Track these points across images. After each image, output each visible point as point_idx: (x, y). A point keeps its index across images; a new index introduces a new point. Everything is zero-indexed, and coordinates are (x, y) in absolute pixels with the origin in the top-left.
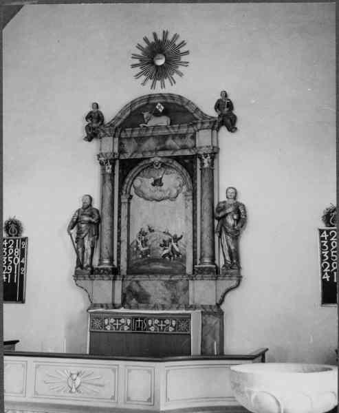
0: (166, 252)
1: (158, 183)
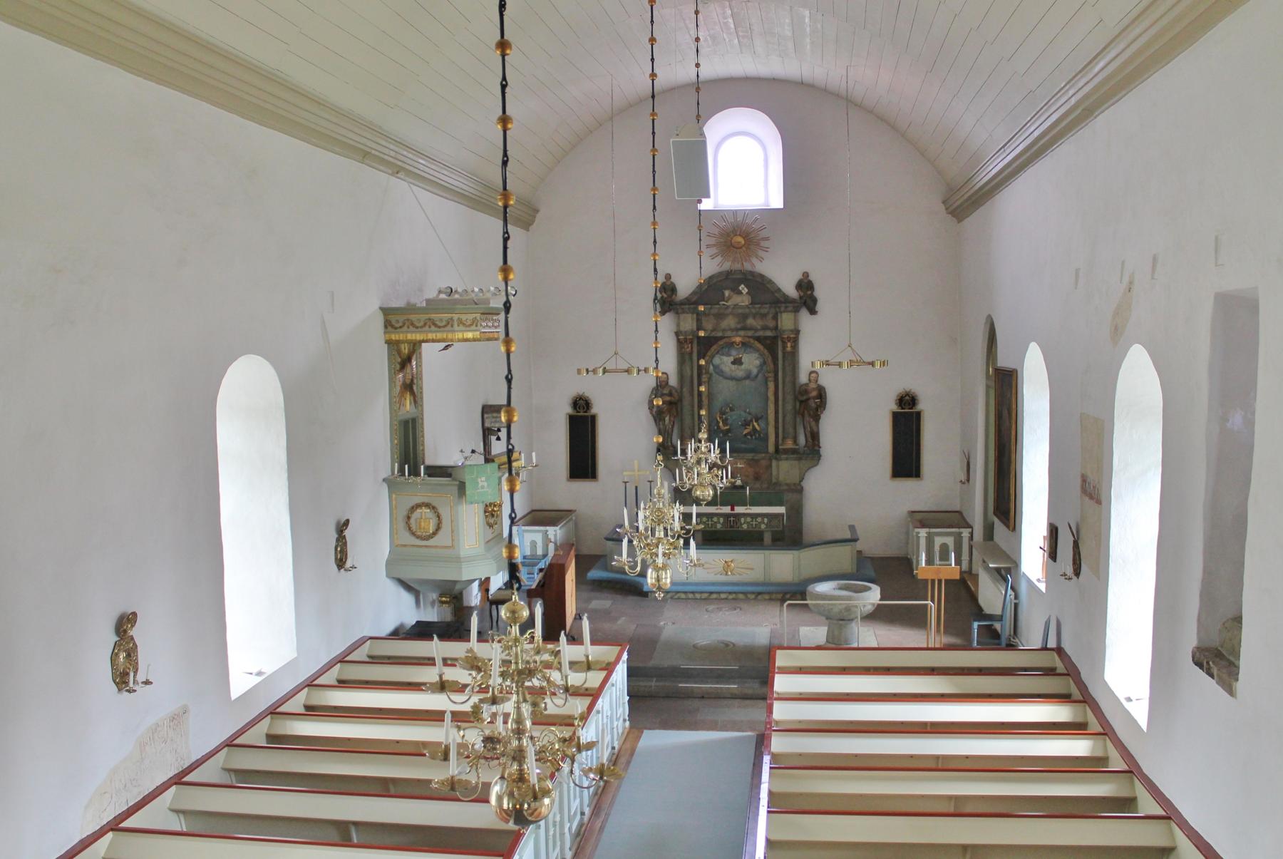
0: (746, 432)
1: (737, 362)
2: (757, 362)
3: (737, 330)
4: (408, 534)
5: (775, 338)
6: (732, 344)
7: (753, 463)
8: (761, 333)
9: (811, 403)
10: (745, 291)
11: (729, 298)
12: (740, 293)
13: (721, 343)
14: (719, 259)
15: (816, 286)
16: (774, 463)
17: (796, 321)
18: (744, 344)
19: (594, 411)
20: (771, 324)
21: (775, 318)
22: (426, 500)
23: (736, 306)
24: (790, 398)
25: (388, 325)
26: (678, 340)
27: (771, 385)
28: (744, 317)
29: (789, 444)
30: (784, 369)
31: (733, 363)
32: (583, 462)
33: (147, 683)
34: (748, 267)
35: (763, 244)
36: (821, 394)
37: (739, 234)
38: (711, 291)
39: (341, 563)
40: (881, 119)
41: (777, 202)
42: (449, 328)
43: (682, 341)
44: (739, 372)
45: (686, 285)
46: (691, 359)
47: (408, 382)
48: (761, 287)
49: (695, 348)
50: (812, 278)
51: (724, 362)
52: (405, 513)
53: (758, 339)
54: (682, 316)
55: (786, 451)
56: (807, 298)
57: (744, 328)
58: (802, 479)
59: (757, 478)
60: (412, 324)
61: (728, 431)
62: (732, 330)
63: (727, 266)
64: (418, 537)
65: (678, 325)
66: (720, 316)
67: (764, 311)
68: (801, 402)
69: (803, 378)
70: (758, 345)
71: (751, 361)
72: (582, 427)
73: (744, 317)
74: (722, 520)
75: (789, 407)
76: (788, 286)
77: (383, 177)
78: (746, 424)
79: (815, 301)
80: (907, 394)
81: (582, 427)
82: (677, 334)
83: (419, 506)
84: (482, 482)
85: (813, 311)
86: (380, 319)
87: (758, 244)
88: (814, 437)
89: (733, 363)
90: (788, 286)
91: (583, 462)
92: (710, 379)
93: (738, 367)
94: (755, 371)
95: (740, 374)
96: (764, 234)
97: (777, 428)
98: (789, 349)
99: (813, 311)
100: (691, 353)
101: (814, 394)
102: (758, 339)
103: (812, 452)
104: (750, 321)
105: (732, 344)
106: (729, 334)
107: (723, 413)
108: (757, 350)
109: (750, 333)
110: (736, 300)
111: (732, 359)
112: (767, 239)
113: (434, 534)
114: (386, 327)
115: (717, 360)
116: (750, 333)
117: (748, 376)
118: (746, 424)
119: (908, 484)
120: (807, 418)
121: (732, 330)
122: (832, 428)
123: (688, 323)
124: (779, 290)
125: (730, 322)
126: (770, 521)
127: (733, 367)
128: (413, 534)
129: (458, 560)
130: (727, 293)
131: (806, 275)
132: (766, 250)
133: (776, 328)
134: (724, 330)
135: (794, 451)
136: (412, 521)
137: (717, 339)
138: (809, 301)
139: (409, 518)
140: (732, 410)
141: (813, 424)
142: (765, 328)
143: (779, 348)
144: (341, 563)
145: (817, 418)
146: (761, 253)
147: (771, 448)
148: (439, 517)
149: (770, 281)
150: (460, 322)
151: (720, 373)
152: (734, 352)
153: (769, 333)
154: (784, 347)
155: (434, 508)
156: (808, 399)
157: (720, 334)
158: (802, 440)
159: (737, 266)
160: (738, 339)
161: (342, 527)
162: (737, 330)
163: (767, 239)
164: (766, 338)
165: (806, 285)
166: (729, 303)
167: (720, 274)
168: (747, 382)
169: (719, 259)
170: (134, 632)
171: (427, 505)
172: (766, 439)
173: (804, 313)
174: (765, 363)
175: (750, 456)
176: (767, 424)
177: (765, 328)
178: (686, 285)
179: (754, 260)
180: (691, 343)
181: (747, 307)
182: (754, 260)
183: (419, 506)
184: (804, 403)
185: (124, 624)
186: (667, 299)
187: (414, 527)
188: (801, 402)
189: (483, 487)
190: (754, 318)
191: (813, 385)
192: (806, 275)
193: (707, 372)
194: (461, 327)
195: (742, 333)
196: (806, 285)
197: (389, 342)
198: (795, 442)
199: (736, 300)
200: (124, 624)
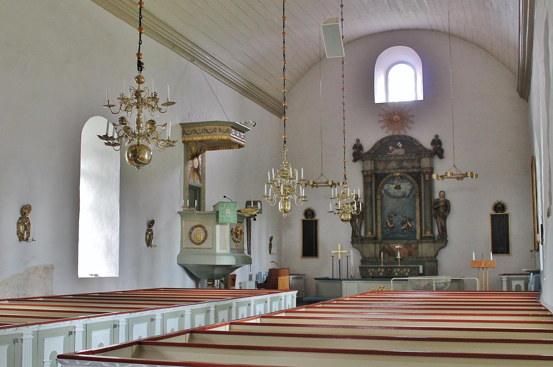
0: (404, 227)
1: (398, 187)
2: (409, 187)
3: (397, 169)
4: (190, 242)
5: (419, 173)
6: (394, 178)
7: (407, 246)
8: (411, 170)
9: (442, 209)
10: (401, 146)
11: (392, 150)
12: (398, 147)
13: (388, 176)
14: (386, 129)
15: (443, 142)
16: (420, 246)
17: (431, 163)
18: (401, 177)
19: (316, 218)
20: (417, 165)
21: (419, 161)
22: (200, 223)
23: (396, 155)
24: (428, 207)
25: (184, 133)
26: (364, 176)
27: (418, 200)
28: (402, 161)
29: (428, 233)
30: (425, 190)
31: (395, 188)
32: (310, 248)
33: (33, 240)
34: (402, 133)
35: (410, 119)
36: (447, 206)
37: (396, 115)
38: (382, 147)
39: (149, 243)
40: (479, 46)
41: (421, 97)
42: (214, 133)
43: (366, 175)
44: (399, 193)
45: (368, 145)
46: (371, 186)
47: (196, 167)
48: (410, 144)
49: (374, 181)
50: (440, 138)
51: (391, 188)
52: (189, 231)
53: (409, 174)
54: (366, 161)
55: (426, 238)
56: (437, 149)
57: (401, 168)
58: (437, 255)
59: (410, 254)
60: (196, 132)
61: (393, 227)
62: (394, 169)
63: (390, 133)
64: (195, 243)
65: (363, 167)
66: (387, 162)
67: (413, 158)
68: (435, 209)
69: (437, 196)
70: (409, 177)
71: (406, 187)
72: (310, 227)
73: (402, 161)
74: (383, 270)
75: (428, 213)
76: (427, 143)
77: (184, 61)
78: (403, 223)
79: (442, 151)
80: (499, 203)
81: (310, 227)
82: (363, 172)
83: (196, 226)
84: (228, 211)
85: (441, 157)
86: (180, 130)
87: (408, 119)
88: (443, 230)
89: (395, 188)
90: (427, 143)
91: (310, 248)
92: (382, 197)
93: (399, 189)
94: (408, 192)
95: (400, 194)
96: (410, 114)
97: (421, 225)
98: (427, 178)
99: (441, 157)
100: (371, 183)
101: (442, 204)
102: (409, 174)
103: (443, 239)
104: (405, 164)
105: (394, 178)
106: (392, 171)
107: (390, 217)
108: (408, 180)
109: (405, 171)
110: (396, 151)
111: (395, 186)
112: (413, 116)
113: (203, 241)
114: (183, 134)
115: (386, 187)
116: (405, 171)
117: (404, 196)
118: (403, 223)
119: (502, 258)
120: (438, 218)
121: (394, 169)
122: (453, 224)
123: (369, 166)
124: (421, 145)
125: (393, 164)
126: (411, 270)
127: (396, 191)
128: (193, 242)
129: (215, 254)
130: (391, 148)
131: (437, 136)
132: (412, 122)
133: (420, 167)
134: (390, 169)
135: (430, 238)
136: (192, 235)
137: (386, 175)
138: (439, 151)
139: (191, 233)
140: (395, 215)
141: (442, 221)
142: (413, 167)
143: (421, 179)
144: (149, 243)
145: (445, 218)
146: (410, 125)
147: (418, 237)
148: (206, 232)
149: (416, 141)
150: (220, 130)
151: (388, 194)
152: (396, 182)
153: (416, 170)
154: (425, 177)
155: (204, 227)
156: (438, 207)
157: (387, 172)
158: (437, 233)
159: (396, 133)
160: (398, 174)
161: (151, 223)
162: (397, 169)
163: (413, 116)
164: (415, 173)
165: (437, 142)
166: (392, 154)
167: (387, 137)
168: (404, 199)
169: (386, 129)
170: (30, 216)
171: (200, 226)
172: (415, 232)
173: (436, 159)
174: (414, 187)
175: (405, 242)
176: (415, 222)
177: (413, 167)
178: (368, 145)
179: (406, 129)
180: (371, 176)
181: (403, 155)
182: (406, 129)
183: (196, 226)
184: (437, 209)
185: (25, 210)
186: (358, 154)
187: (193, 237)
188: (435, 209)
189: (228, 214)
190: (407, 162)
191: (442, 199)
192: (437, 136)
193: (381, 193)
194: (221, 133)
195: (400, 170)
196: (437, 142)
197: (183, 142)
198: (432, 231)
199: (396, 151)
200: (25, 210)
